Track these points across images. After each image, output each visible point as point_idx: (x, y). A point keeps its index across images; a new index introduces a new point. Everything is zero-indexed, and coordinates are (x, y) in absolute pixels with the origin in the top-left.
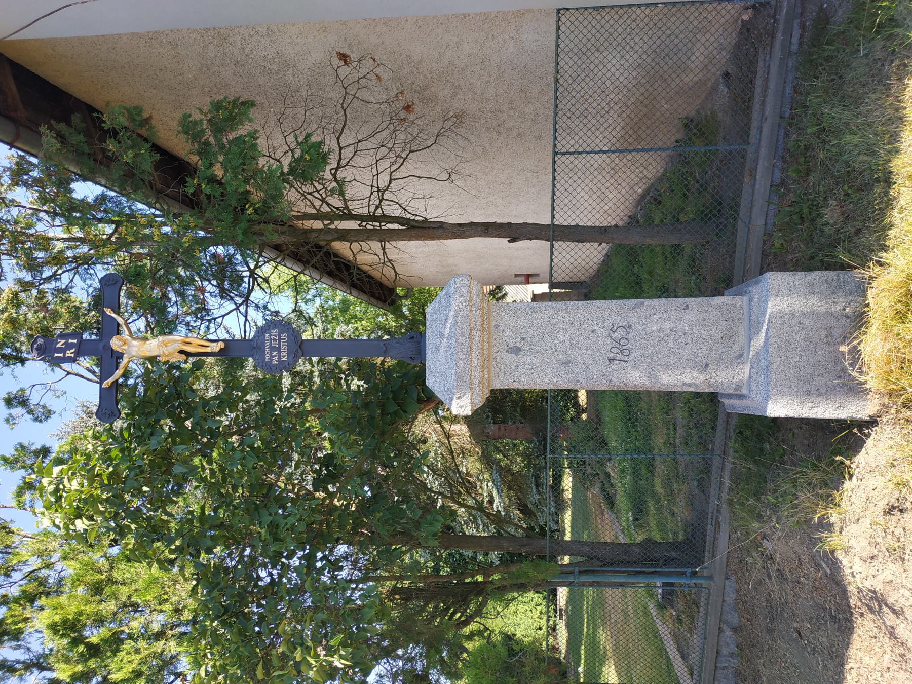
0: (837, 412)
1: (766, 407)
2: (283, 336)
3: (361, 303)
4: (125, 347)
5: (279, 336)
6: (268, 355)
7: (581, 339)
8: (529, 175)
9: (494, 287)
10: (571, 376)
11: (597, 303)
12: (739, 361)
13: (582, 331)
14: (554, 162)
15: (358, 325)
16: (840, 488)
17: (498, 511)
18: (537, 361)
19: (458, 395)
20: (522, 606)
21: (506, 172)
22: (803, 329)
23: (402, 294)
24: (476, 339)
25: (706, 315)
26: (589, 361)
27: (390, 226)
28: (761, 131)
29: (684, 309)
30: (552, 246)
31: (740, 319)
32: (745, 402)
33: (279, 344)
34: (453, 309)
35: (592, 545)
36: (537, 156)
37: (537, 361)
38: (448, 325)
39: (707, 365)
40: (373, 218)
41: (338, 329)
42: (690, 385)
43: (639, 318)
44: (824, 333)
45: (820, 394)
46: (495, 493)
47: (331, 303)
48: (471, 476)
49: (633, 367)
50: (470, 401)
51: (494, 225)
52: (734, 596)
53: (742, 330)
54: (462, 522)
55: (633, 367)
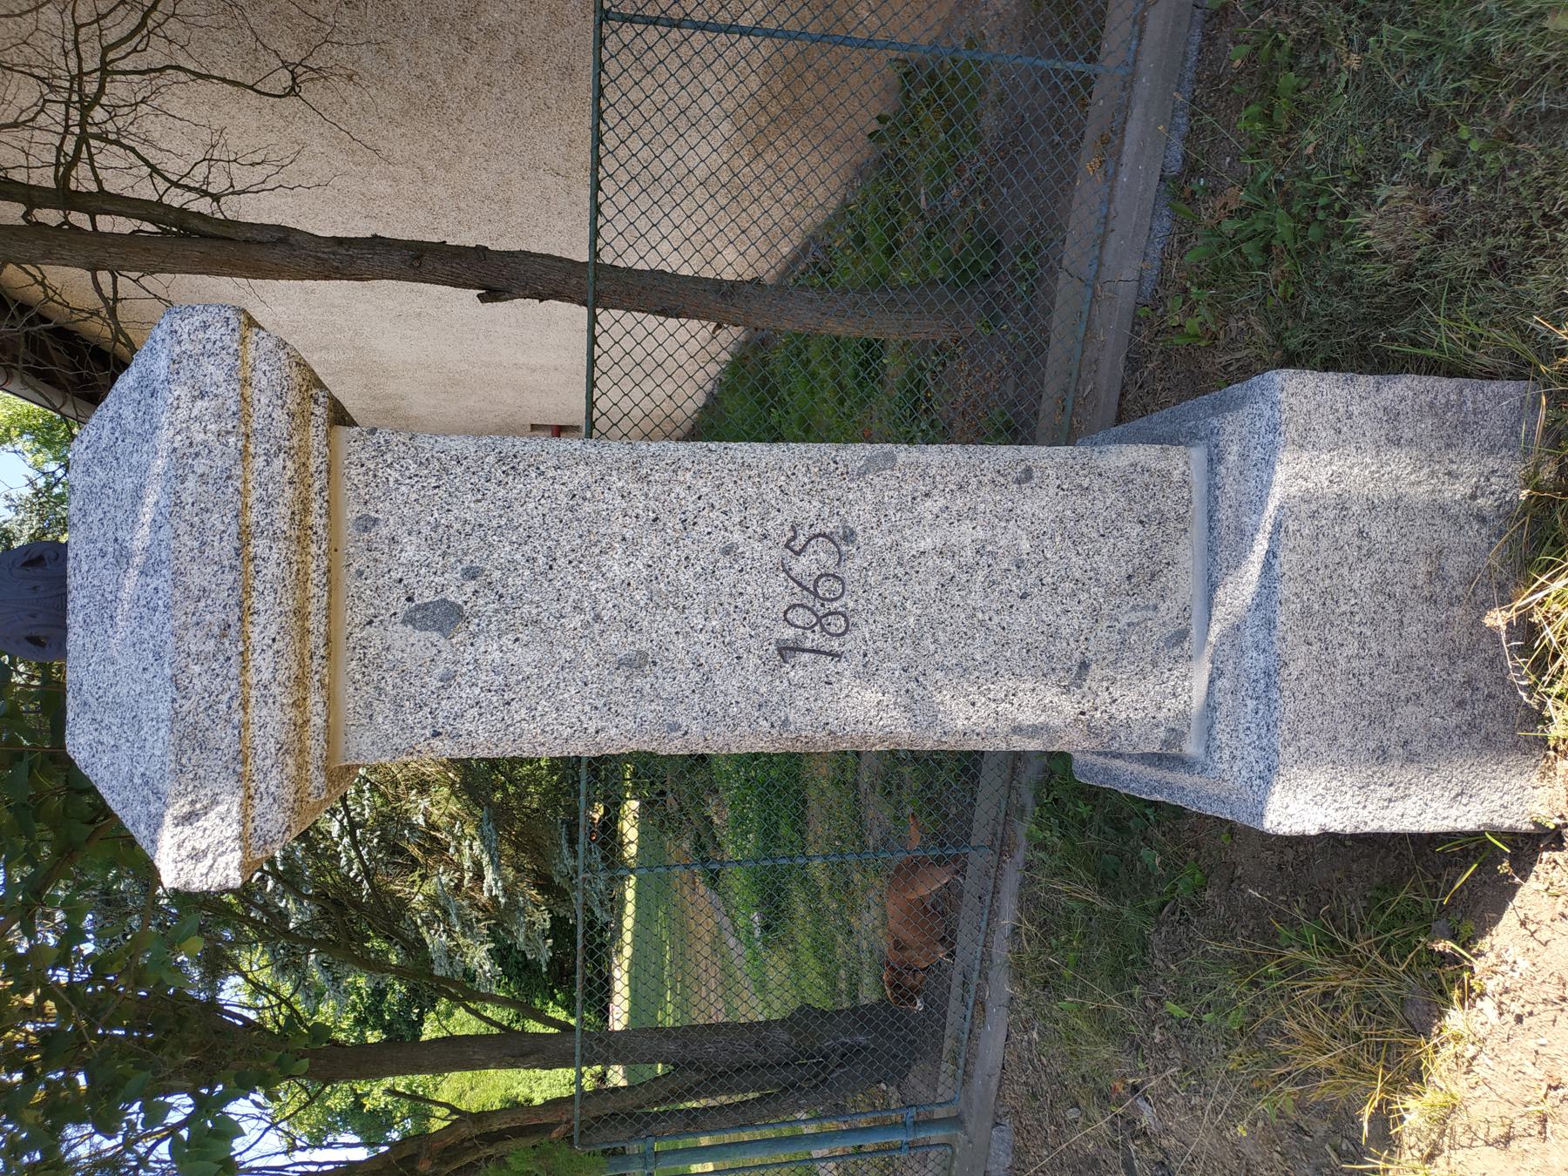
0: (1454, 812)
1: (1262, 803)
7: (686, 576)
8: (549, 180)
10: (648, 710)
11: (743, 451)
12: (1177, 651)
13: (690, 549)
14: (600, 42)
16: (1435, 1030)
17: (494, 899)
18: (524, 657)
19: (181, 807)
21: (494, 166)
22: (1369, 554)
24: (270, 571)
25: (1082, 504)
26: (715, 657)
27: (105, 223)
28: (1142, 31)
29: (1019, 482)
30: (593, 320)
31: (1180, 518)
32: (1181, 778)
34: (164, 447)
35: (685, 1033)
36: (566, 128)
37: (524, 657)
38: (147, 514)
39: (1084, 666)
42: (1035, 731)
43: (879, 505)
44: (1423, 567)
45: (1411, 758)
48: (438, 830)
49: (857, 675)
50: (235, 829)
52: (1007, 1161)
53: (1187, 554)
54: (419, 921)
55: (857, 675)
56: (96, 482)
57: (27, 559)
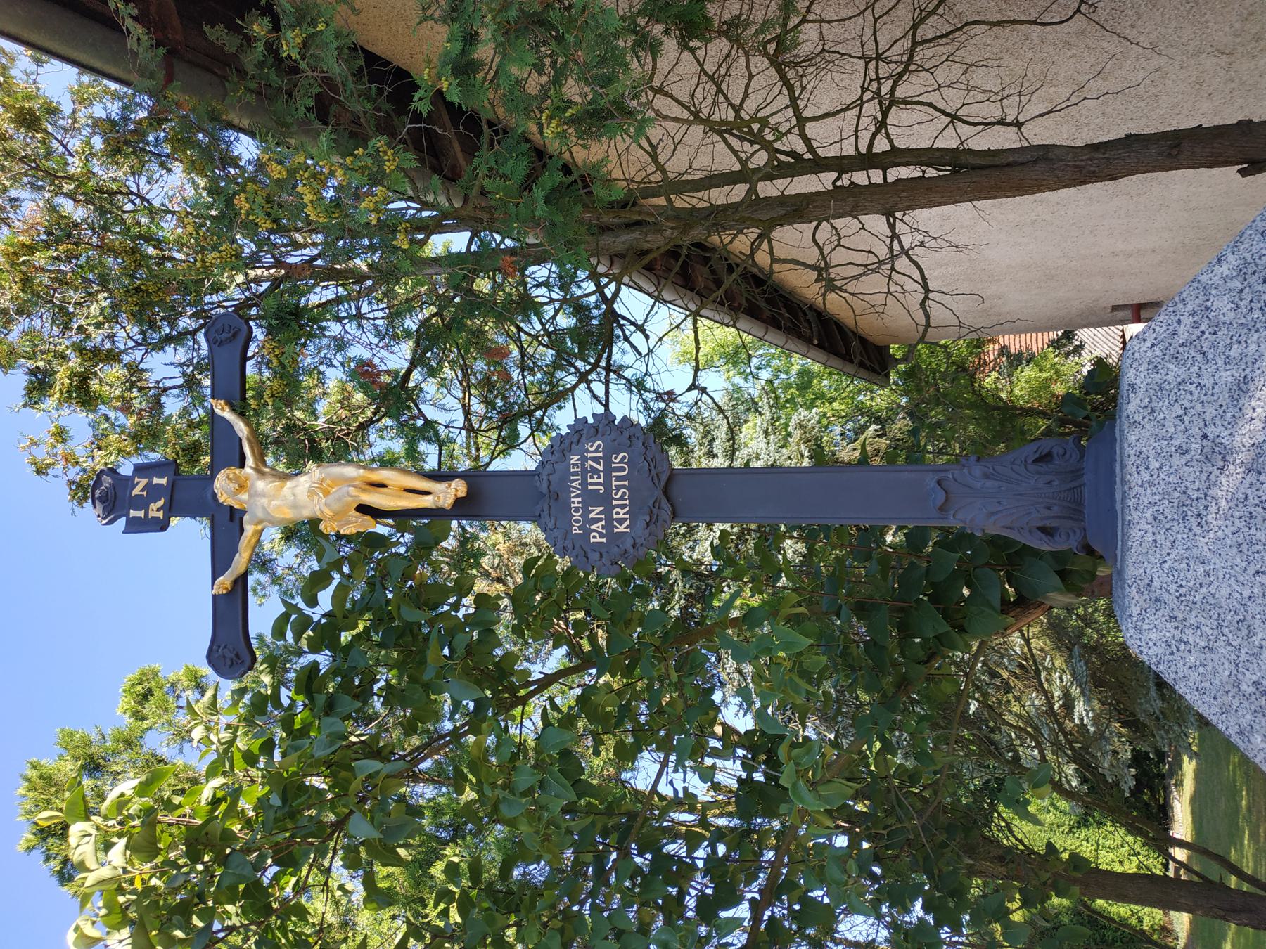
2: (617, 460)
3: (831, 374)
4: (244, 496)
5: (607, 462)
6: (577, 516)
9: (1060, 333)
15: (827, 409)
17: (1082, 726)
20: (1104, 852)
23: (899, 355)
27: (894, 174)
33: (607, 484)
40: (868, 160)
41: (794, 417)
46: (1075, 691)
47: (783, 376)
51: (1197, 133)
56: (1170, 378)
57: (1037, 455)
